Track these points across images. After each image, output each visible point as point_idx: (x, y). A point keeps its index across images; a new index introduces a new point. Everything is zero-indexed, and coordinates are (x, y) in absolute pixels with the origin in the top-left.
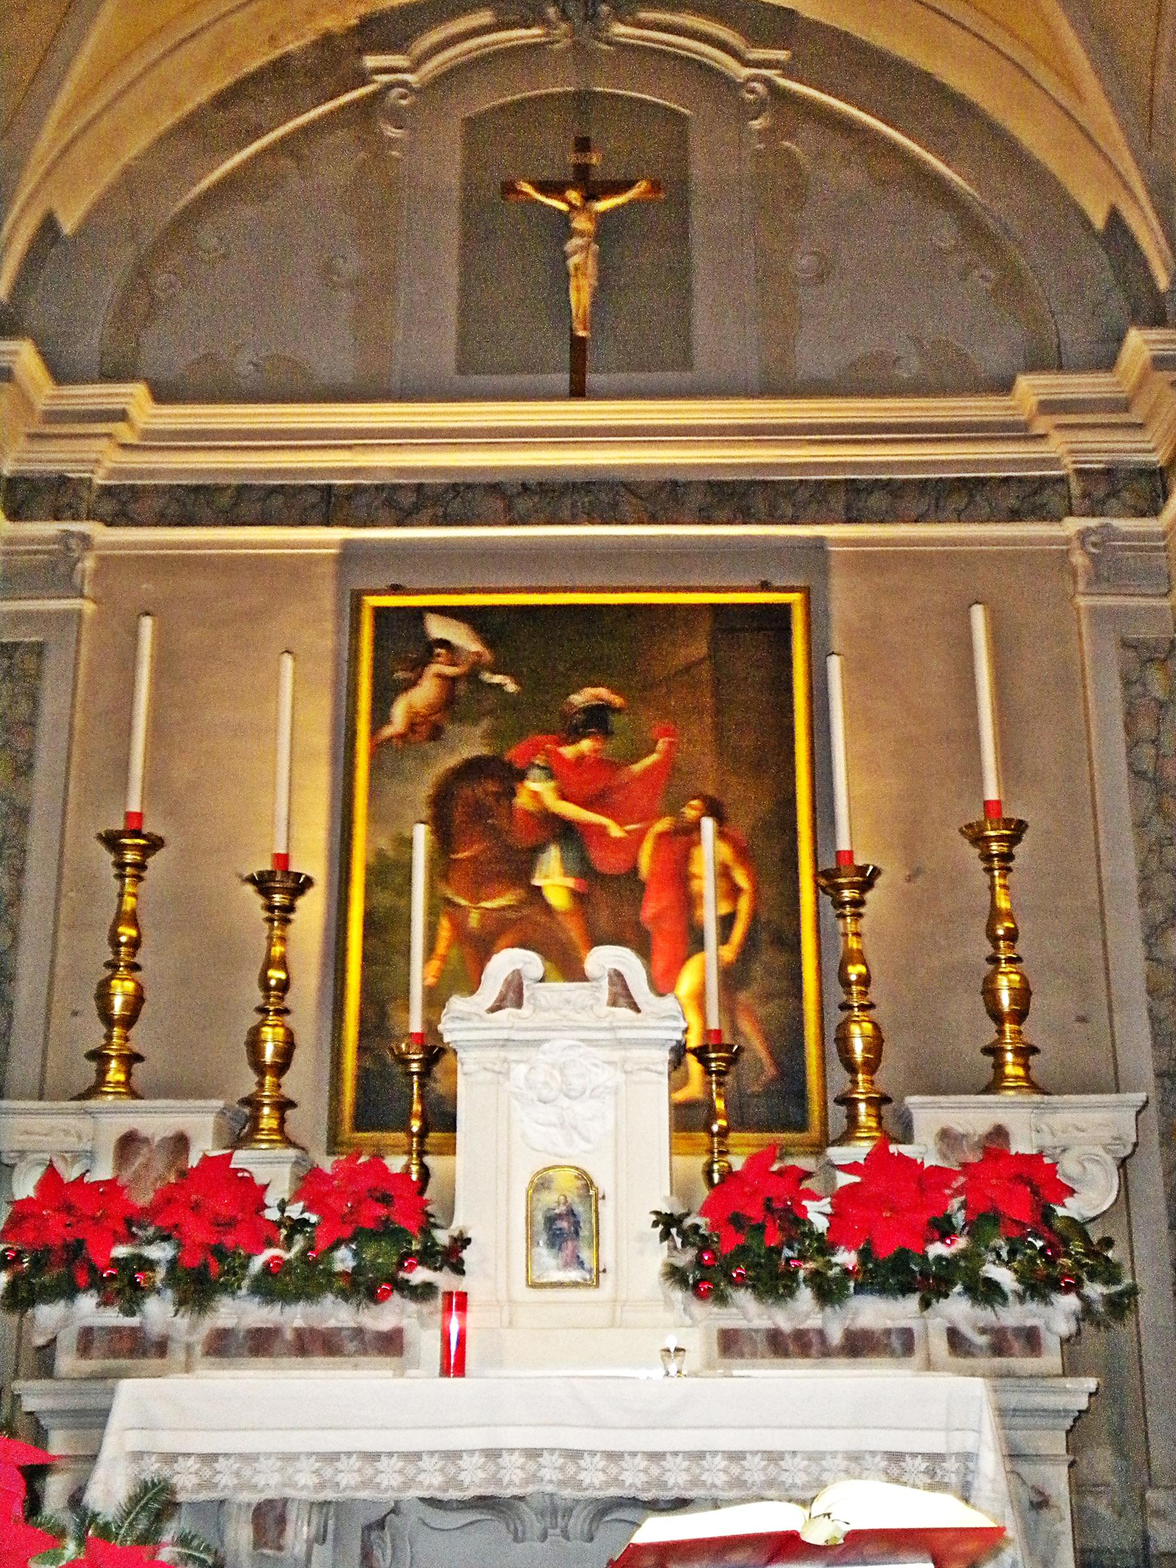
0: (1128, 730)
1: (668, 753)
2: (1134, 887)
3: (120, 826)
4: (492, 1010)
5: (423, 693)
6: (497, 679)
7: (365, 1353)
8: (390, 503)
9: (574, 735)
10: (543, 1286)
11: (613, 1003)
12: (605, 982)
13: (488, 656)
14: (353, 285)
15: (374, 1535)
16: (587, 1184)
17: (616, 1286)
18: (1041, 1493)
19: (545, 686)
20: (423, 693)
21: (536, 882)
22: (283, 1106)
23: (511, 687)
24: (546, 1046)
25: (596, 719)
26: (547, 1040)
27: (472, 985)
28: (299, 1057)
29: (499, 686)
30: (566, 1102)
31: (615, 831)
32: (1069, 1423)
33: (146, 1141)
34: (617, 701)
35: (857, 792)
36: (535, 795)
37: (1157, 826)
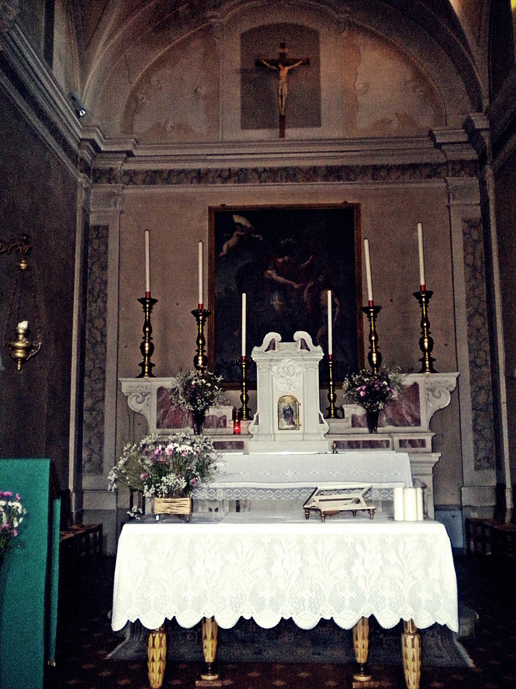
1: (312, 260)
4: (266, 351)
5: (232, 242)
6: (257, 236)
7: (232, 448)
8: (220, 176)
12: (300, 342)
14: (205, 97)
16: (295, 401)
17: (304, 429)
18: (424, 484)
20: (232, 242)
21: (272, 303)
22: (151, 365)
24: (282, 361)
26: (283, 359)
27: (260, 344)
28: (155, 351)
31: (296, 286)
32: (433, 465)
36: (271, 275)
37: (473, 282)
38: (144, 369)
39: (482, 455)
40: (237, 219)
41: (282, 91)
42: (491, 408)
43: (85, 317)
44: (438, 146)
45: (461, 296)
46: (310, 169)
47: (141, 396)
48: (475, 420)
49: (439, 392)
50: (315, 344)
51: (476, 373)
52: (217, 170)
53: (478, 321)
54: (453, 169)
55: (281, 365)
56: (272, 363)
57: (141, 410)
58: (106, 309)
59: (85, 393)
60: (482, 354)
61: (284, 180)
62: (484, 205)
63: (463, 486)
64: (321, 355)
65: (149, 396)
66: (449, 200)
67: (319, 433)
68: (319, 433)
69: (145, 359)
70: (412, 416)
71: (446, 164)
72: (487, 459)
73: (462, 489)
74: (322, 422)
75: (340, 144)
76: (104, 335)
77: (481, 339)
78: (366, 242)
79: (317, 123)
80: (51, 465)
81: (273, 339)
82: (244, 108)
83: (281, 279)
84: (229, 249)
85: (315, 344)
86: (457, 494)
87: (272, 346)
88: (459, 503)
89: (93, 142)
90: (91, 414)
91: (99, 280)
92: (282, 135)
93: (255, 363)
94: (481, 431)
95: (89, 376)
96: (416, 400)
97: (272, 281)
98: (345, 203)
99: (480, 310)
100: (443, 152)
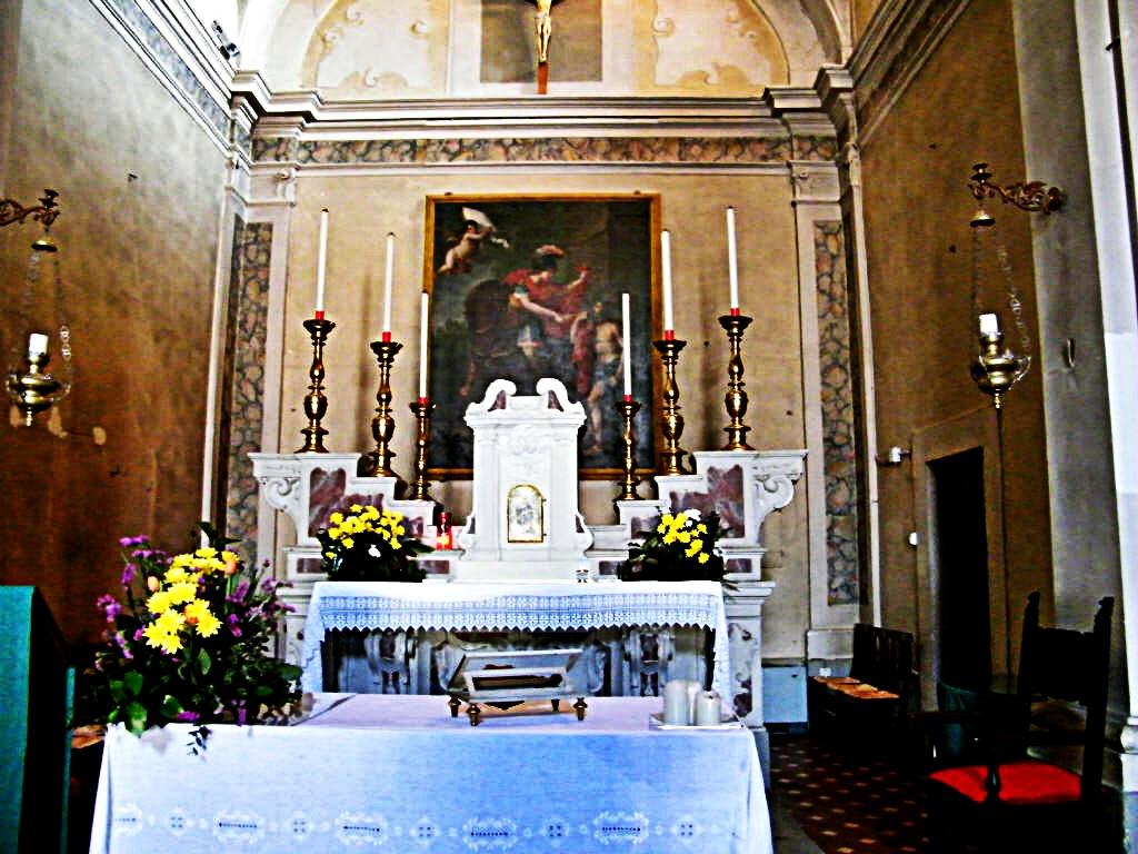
0: (817, 267)
2: (817, 349)
3: (313, 317)
4: (489, 410)
5: (462, 248)
6: (500, 241)
8: (445, 151)
9: (537, 269)
10: (514, 542)
11: (550, 407)
13: (494, 230)
15: (437, 653)
19: (524, 247)
20: (462, 248)
21: (520, 344)
23: (506, 245)
25: (549, 262)
28: (396, 432)
29: (501, 244)
30: (525, 454)
31: (559, 319)
33: (325, 473)
34: (560, 252)
35: (684, 298)
36: (518, 300)
38: (308, 440)
39: (838, 582)
40: (469, 214)
41: (542, 26)
42: (854, 510)
43: (232, 362)
44: (778, 113)
45: (812, 338)
46: (583, 144)
47: (285, 483)
48: (830, 530)
49: (776, 483)
50: (572, 400)
51: (833, 457)
52: (441, 142)
53: (838, 377)
54: (800, 149)
55: (515, 433)
56: (500, 431)
57: (285, 507)
58: (263, 351)
59: (230, 483)
60: (843, 428)
61: (544, 157)
62: (846, 200)
63: (810, 628)
64: (580, 419)
65: (298, 483)
66: (794, 193)
67: (576, 548)
68: (576, 548)
69: (311, 423)
70: (730, 520)
71: (790, 140)
72: (847, 587)
73: (809, 634)
74: (580, 530)
75: (627, 106)
76: (259, 392)
77: (841, 404)
78: (665, 237)
79: (597, 76)
80: (38, 602)
81: (502, 392)
82: (484, 52)
83: (535, 308)
84: (456, 261)
85: (572, 400)
86: (800, 645)
87: (500, 402)
88: (803, 655)
89: (250, 96)
90: (239, 514)
91: (254, 308)
92: (543, 91)
93: (472, 431)
94: (838, 545)
95: (236, 455)
96: (738, 494)
97: (521, 309)
98: (637, 193)
99: (841, 361)
100: (785, 123)
